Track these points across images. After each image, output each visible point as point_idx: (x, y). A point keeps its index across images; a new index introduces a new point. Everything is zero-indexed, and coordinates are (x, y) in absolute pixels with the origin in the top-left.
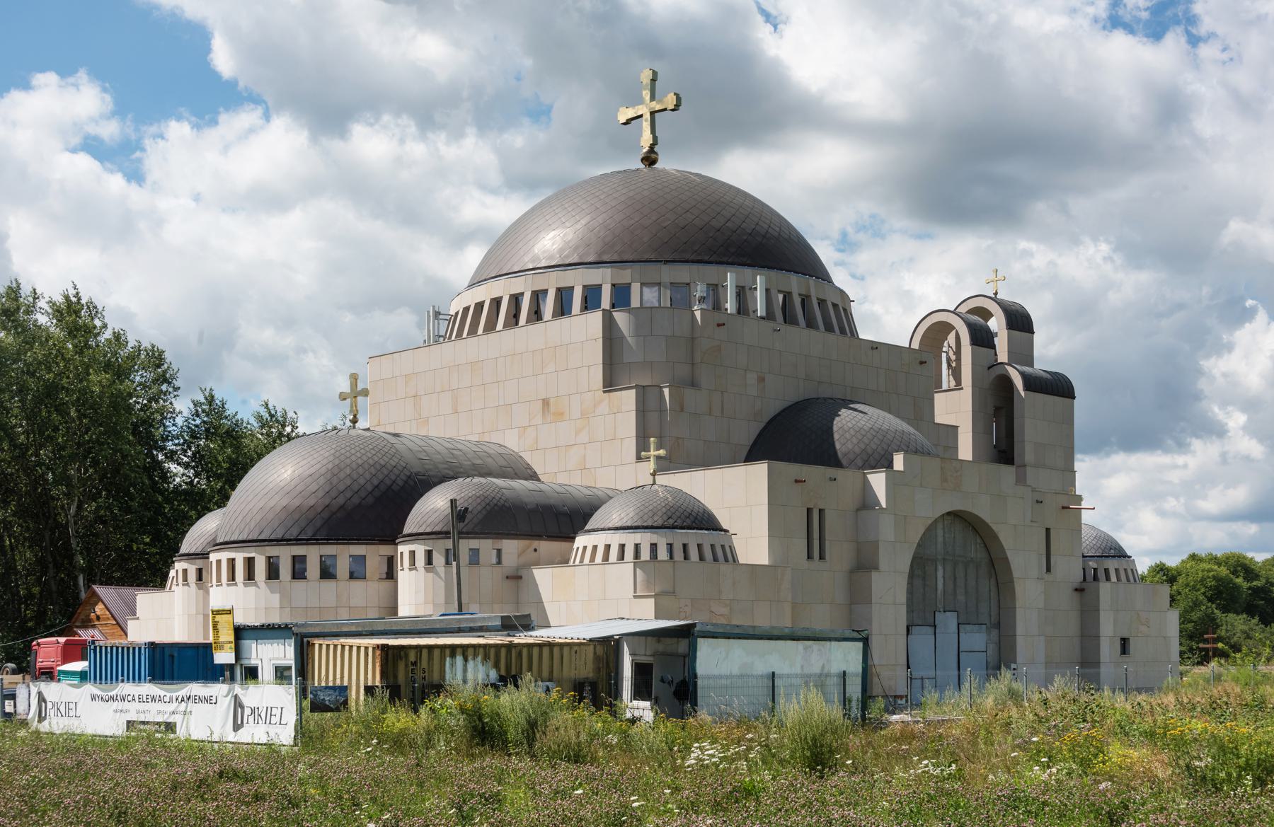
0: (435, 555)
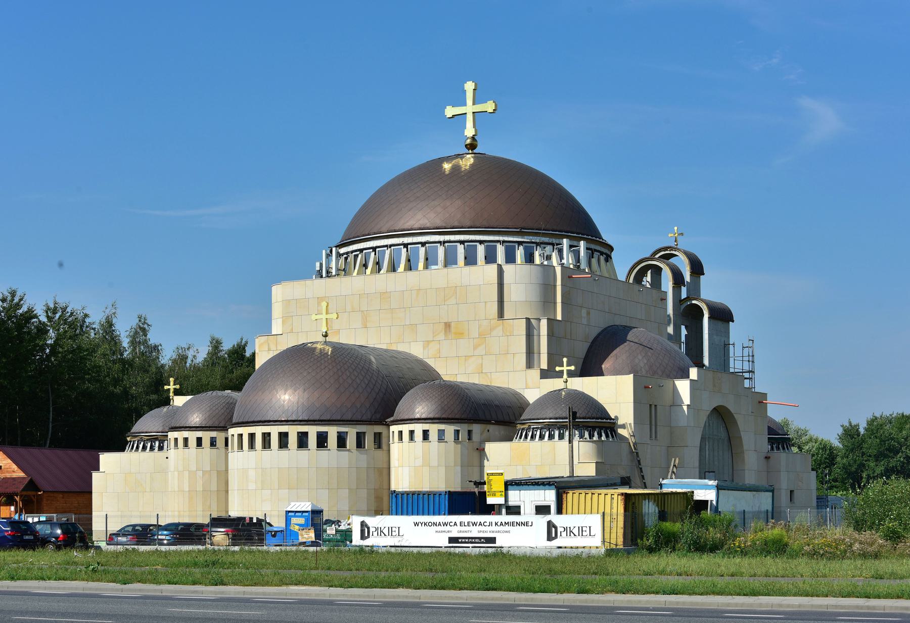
0: (416, 434)
